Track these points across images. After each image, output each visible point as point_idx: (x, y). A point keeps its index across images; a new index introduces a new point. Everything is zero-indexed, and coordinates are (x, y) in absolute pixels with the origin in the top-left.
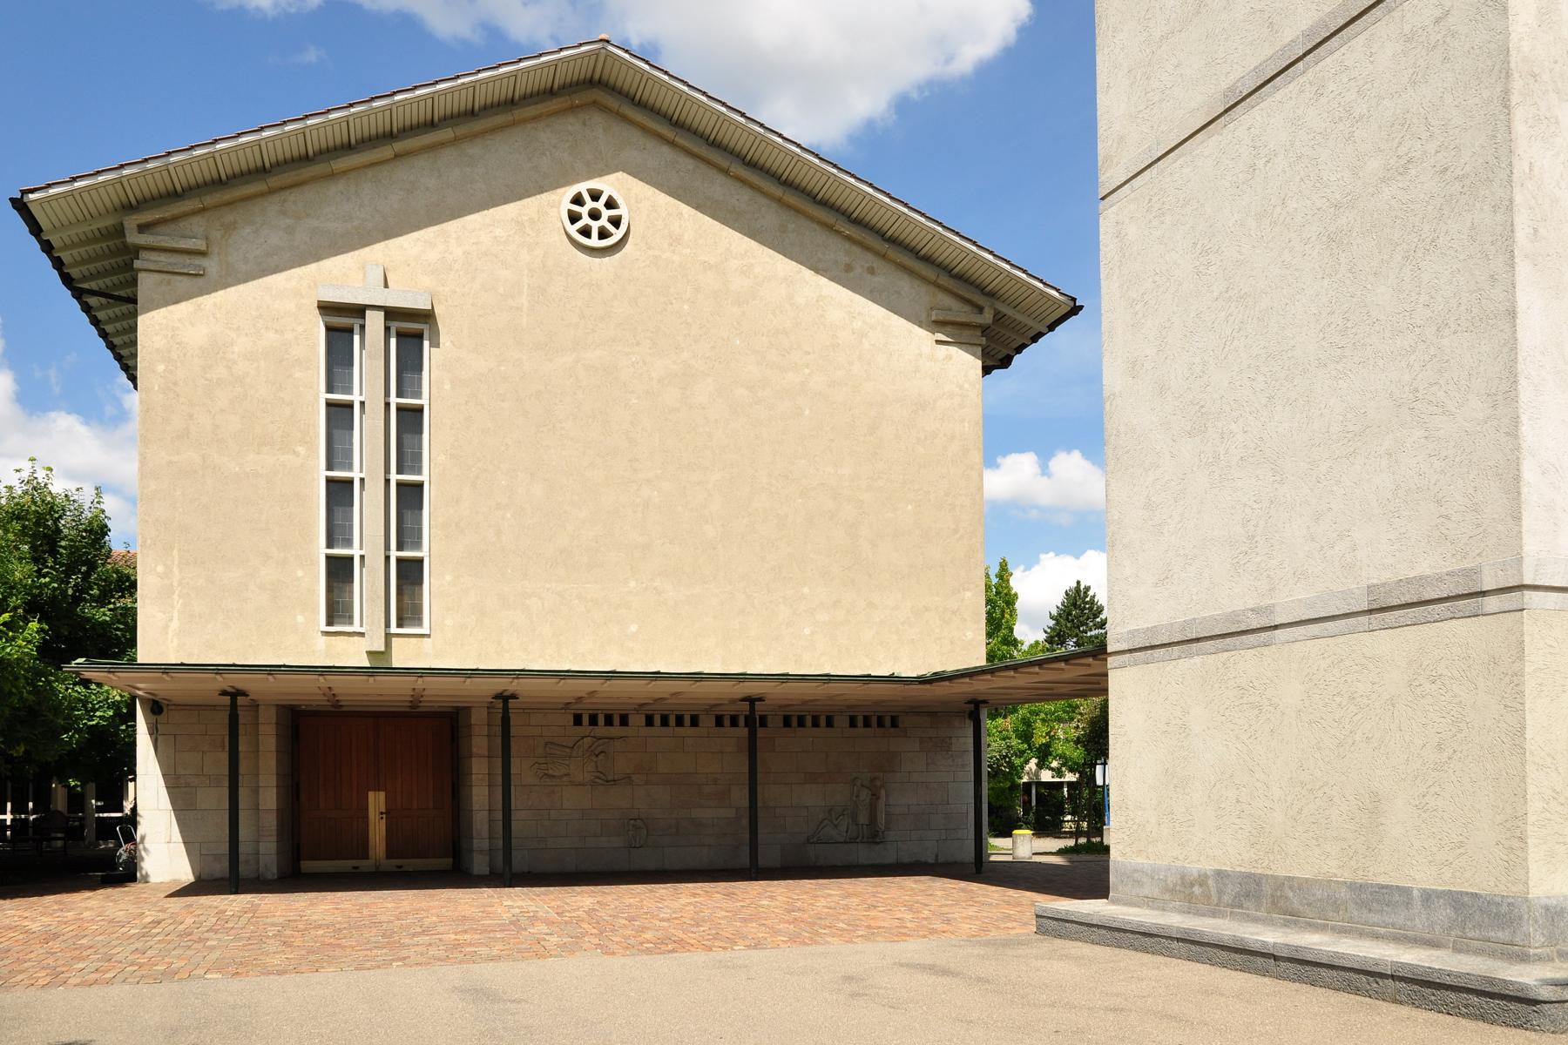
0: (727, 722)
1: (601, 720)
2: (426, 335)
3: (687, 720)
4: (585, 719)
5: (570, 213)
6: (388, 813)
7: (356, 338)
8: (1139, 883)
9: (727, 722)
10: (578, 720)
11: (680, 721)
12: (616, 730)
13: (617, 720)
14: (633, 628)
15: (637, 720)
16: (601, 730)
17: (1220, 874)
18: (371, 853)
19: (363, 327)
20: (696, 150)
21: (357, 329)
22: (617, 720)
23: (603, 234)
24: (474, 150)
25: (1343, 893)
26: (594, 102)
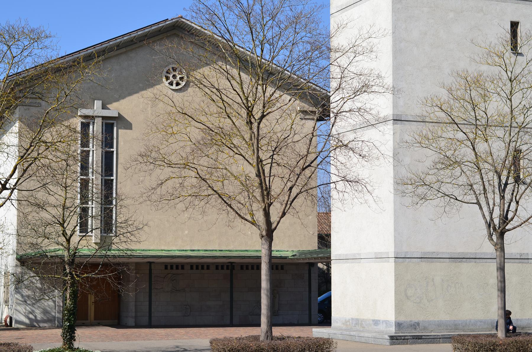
0: (220, 268)
1: (174, 267)
2: (115, 124)
3: (205, 267)
4: (169, 267)
5: (169, 83)
6: (95, 302)
7: (91, 127)
8: (337, 322)
9: (220, 268)
10: (166, 267)
11: (203, 268)
12: (180, 271)
13: (180, 267)
14: (186, 232)
15: (187, 267)
16: (175, 271)
17: (352, 319)
18: (89, 318)
19: (94, 123)
20: (246, 253)
21: (91, 123)
22: (180, 267)
23: (178, 84)
24: (132, 55)
25: (371, 322)
26: (175, 34)
